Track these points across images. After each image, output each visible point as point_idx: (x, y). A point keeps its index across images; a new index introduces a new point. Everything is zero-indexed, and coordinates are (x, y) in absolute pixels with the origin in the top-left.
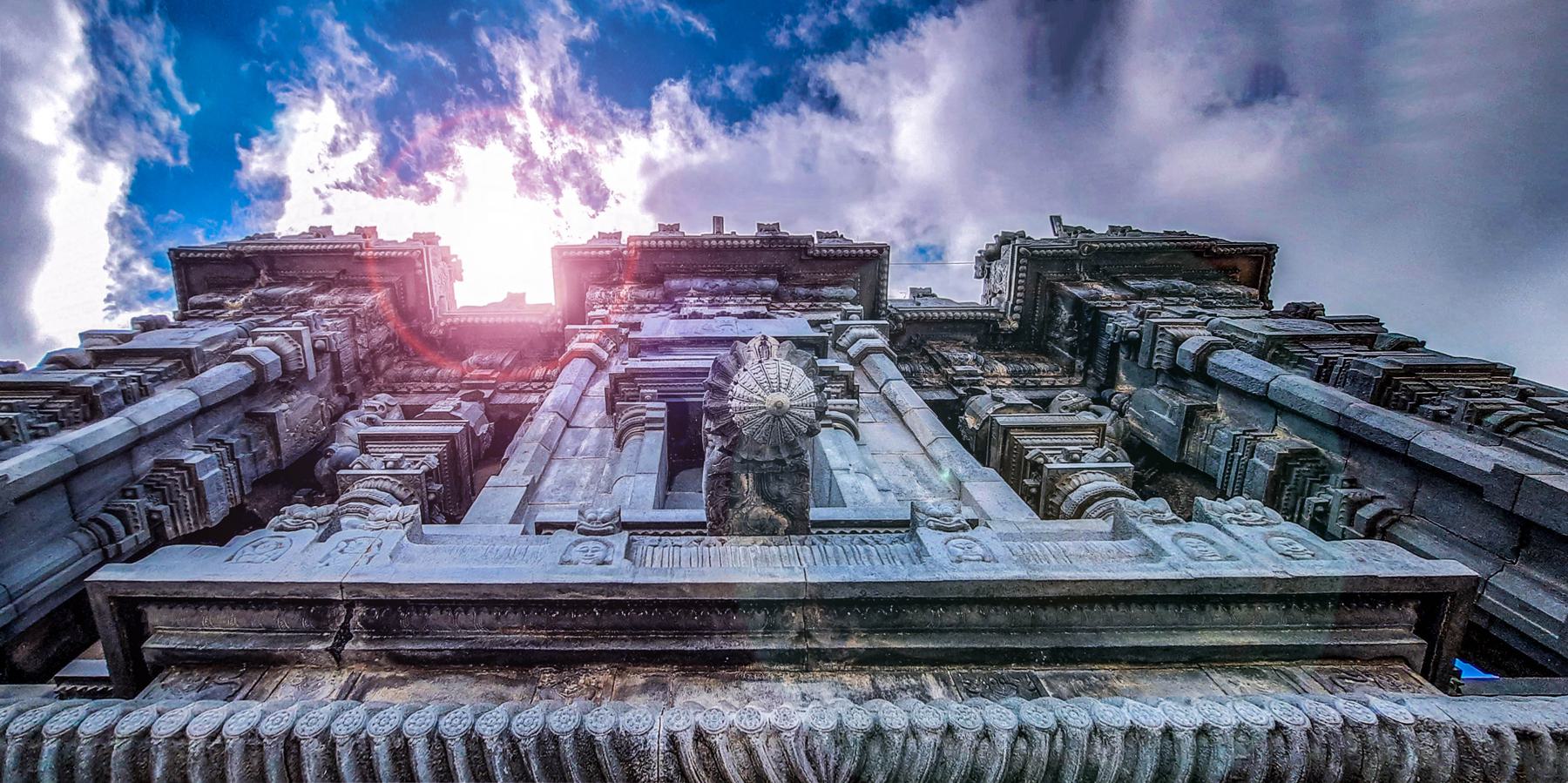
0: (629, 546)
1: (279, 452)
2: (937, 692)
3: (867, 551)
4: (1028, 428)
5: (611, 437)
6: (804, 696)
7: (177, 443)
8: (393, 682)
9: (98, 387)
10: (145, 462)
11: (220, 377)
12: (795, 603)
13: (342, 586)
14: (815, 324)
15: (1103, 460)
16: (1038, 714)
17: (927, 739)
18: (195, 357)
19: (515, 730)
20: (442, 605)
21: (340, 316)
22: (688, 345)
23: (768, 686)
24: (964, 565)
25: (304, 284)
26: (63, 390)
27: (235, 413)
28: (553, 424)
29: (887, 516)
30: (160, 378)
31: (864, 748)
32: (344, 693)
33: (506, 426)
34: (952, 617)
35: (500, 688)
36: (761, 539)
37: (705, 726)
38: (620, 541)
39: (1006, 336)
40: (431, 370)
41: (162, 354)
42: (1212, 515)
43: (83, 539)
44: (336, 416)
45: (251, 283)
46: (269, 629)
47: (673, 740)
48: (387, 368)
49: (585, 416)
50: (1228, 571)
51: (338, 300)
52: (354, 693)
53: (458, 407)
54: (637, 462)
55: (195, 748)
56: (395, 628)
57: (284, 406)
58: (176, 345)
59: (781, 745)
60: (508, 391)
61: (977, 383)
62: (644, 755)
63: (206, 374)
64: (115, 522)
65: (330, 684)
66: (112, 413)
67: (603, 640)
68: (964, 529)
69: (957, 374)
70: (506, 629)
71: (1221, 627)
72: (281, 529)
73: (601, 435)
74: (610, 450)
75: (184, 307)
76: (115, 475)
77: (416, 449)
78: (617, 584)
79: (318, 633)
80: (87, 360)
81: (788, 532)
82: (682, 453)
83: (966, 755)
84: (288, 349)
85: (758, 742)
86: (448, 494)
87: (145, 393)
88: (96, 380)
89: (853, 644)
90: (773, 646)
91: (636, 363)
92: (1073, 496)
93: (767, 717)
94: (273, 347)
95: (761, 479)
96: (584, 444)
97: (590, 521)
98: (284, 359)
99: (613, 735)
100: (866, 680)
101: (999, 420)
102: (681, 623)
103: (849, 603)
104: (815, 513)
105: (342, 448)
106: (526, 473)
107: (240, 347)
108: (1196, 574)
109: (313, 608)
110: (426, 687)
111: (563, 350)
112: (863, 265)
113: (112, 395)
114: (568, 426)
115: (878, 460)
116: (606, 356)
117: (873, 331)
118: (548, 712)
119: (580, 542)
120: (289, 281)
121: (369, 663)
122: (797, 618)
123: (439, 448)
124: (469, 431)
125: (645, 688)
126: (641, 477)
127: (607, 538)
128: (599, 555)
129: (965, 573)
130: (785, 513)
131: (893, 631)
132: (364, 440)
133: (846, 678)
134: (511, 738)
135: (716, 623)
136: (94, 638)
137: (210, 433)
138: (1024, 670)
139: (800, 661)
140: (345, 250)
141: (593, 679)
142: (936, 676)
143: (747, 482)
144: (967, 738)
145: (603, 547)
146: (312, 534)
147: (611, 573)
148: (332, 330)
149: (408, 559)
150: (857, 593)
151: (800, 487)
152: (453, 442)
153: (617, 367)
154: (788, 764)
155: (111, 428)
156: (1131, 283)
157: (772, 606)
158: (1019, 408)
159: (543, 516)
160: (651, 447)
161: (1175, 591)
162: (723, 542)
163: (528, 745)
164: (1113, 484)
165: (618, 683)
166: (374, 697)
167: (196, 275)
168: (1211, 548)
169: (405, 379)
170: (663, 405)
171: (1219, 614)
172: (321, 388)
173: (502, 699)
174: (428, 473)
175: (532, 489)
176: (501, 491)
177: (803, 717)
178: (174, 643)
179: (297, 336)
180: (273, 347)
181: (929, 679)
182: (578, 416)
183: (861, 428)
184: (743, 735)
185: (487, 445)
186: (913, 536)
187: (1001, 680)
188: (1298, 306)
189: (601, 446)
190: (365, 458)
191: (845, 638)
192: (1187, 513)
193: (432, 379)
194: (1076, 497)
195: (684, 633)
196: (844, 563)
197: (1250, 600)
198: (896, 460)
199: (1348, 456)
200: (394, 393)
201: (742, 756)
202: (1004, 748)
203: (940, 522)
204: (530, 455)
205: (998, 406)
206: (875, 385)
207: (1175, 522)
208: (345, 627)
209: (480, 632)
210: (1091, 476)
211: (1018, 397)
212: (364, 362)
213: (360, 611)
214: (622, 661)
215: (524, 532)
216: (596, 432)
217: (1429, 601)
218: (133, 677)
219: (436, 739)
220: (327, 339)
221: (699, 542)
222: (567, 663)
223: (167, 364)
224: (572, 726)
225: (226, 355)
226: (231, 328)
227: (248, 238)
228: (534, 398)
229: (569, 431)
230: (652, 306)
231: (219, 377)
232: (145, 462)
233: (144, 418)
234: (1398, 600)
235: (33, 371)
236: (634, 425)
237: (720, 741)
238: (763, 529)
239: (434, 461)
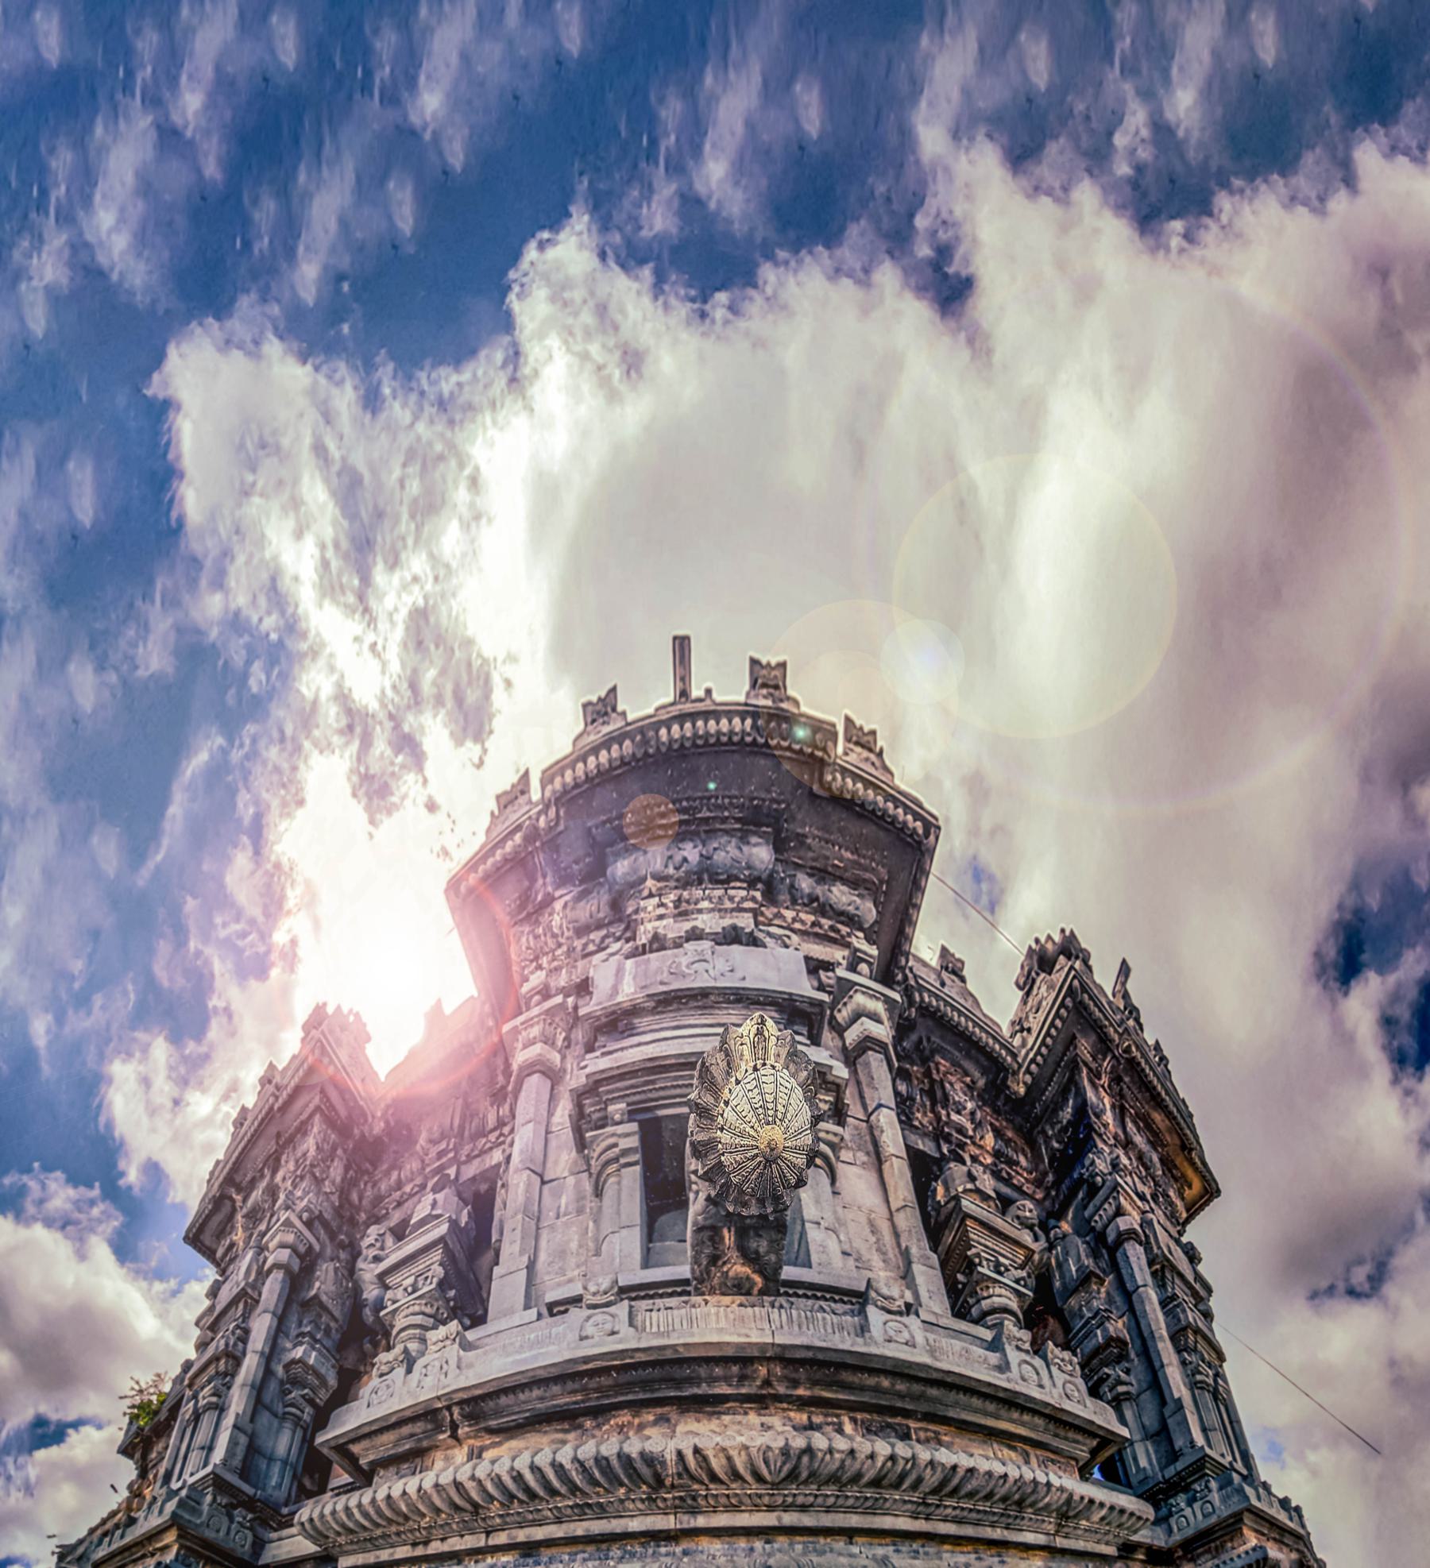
0: (630, 1313)
1: (336, 1320)
2: (848, 1428)
3: (824, 1319)
4: (982, 1224)
5: (588, 1187)
6: (762, 1425)
7: (284, 1350)
8: (494, 1445)
9: (227, 1345)
10: (280, 1370)
11: (271, 1290)
12: (763, 1359)
13: (438, 1398)
14: (815, 967)
15: (1017, 1281)
16: (902, 1450)
17: (837, 1456)
18: (249, 1291)
19: (580, 1457)
20: (506, 1391)
21: (302, 1178)
22: (653, 1011)
23: (739, 1418)
24: (892, 1345)
25: (262, 1176)
26: (216, 1359)
27: (295, 1307)
28: (529, 1185)
29: (844, 1284)
30: (246, 1317)
31: (799, 1458)
32: (470, 1458)
33: (482, 1202)
34: (871, 1381)
35: (560, 1436)
36: (739, 1299)
37: (700, 1445)
38: (622, 1309)
39: (1008, 1098)
40: (394, 1175)
41: (234, 1302)
42: (1050, 1355)
43: (288, 1425)
44: (351, 1270)
45: (234, 1211)
46: (412, 1435)
47: (680, 1454)
48: (361, 1199)
49: (556, 1162)
50: (1036, 1393)
51: (291, 1166)
52: (476, 1454)
53: (434, 1204)
54: (618, 1213)
55: (414, 1496)
56: (482, 1411)
57: (317, 1284)
58: (235, 1291)
59: (749, 1455)
60: (470, 1158)
61: (962, 1146)
62: (663, 1463)
63: (263, 1297)
64: (293, 1410)
65: (460, 1455)
66: (244, 1354)
67: (622, 1394)
68: (900, 1313)
69: (949, 1123)
70: (553, 1397)
71: (1013, 1421)
72: (381, 1375)
73: (577, 1184)
74: (590, 1203)
75: (217, 1264)
76: (273, 1386)
77: (419, 1266)
78: (627, 1350)
79: (439, 1429)
80: (210, 1334)
81: (763, 1292)
82: (663, 1196)
83: (857, 1465)
84: (290, 1238)
85: (734, 1453)
86: (465, 1299)
87: (247, 1332)
88: (222, 1342)
89: (801, 1392)
90: (744, 1391)
91: (598, 1063)
92: (983, 1303)
93: (740, 1439)
94: (282, 1246)
95: (742, 1233)
96: (563, 1201)
97: (594, 1294)
98: (294, 1250)
99: (642, 1454)
100: (805, 1417)
101: (964, 1202)
102: (677, 1376)
103: (802, 1362)
104: (789, 1272)
105: (371, 1293)
106: (521, 1253)
107: (265, 1262)
108: (1018, 1388)
109: (429, 1415)
110: (515, 1444)
111: (507, 1072)
112: (893, 845)
113: (235, 1344)
114: (543, 1183)
115: (849, 1215)
116: (556, 1058)
117: (879, 1007)
118: (598, 1445)
119: (589, 1317)
120: (253, 1183)
121: (475, 1437)
122: (763, 1371)
123: (437, 1255)
124: (454, 1223)
125: (655, 1423)
126: (624, 1232)
127: (612, 1309)
128: (608, 1327)
129: (890, 1351)
130: (761, 1272)
131: (828, 1385)
132: (382, 1277)
133: (792, 1414)
134: (579, 1461)
136: (330, 1463)
137: (293, 1332)
138: (904, 1422)
139: (761, 1401)
140: (267, 1114)
141: (619, 1421)
142: (851, 1418)
143: (728, 1237)
144: (861, 1456)
145: (609, 1318)
146: (400, 1371)
147: (620, 1341)
148: (306, 1198)
149: (470, 1366)
150: (810, 1354)
151: (776, 1246)
152: (446, 1244)
153: (576, 1079)
154: (752, 1465)
155: (250, 1364)
157: (742, 1360)
158: (985, 1197)
159: (550, 1297)
160: (628, 1185)
161: (1001, 1395)
162: (706, 1302)
163: (590, 1463)
164: (1014, 1305)
165: (637, 1421)
166: (488, 1455)
167: (207, 1238)
168: (1035, 1377)
169: (378, 1199)
170: (634, 1127)
171: (1016, 1415)
172: (329, 1251)
173: (564, 1442)
174: (441, 1284)
175: (531, 1267)
176: (506, 1286)
177: (759, 1440)
178: (372, 1458)
179: (288, 1223)
180: (282, 1246)
181: (846, 1419)
182: (549, 1165)
183: (841, 1168)
184: (724, 1450)
185: (473, 1233)
186: (862, 1312)
187: (889, 1425)
188: (1193, 1248)
189: (580, 1198)
190: (389, 1294)
191: (795, 1387)
192: (1037, 1349)
193: (399, 1185)
194: (985, 1304)
195: (678, 1383)
196: (804, 1328)
197: (1035, 1412)
198: (863, 1220)
200: (377, 1220)
201: (724, 1461)
202: (879, 1464)
203: (886, 1304)
204: (518, 1232)
205: (969, 1186)
206: (864, 1106)
207: (1027, 1352)
208: (452, 1421)
209: (534, 1401)
210: (1003, 1292)
211: (987, 1183)
212: (341, 1206)
213: (456, 1411)
214: (637, 1406)
215: (540, 1316)
216: (571, 1180)
217: (1105, 1439)
218: (365, 1477)
219: (534, 1468)
220: (307, 1209)
221: (686, 1302)
222: (599, 1413)
223: (241, 1306)
224: (615, 1451)
225: (263, 1275)
226: (250, 1255)
227: (209, 1181)
228: (497, 1156)
229: (546, 1187)
230: (596, 936)
231: (271, 1291)
232: (280, 1370)
233: (259, 1346)
234: (1092, 1435)
235: (198, 1359)
236: (608, 1163)
237: (710, 1453)
238: (740, 1288)
239: (439, 1271)
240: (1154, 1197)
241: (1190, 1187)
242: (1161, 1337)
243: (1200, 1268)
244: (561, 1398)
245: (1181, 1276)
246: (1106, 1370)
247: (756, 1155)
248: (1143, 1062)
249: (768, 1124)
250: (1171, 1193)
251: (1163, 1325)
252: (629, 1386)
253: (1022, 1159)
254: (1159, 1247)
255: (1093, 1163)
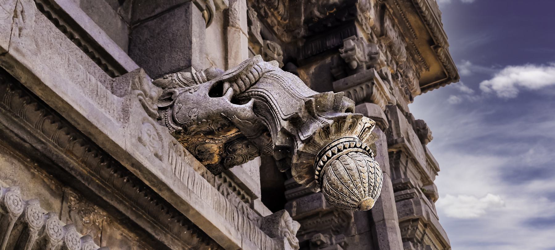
70: (69, 152)
81: (209, 167)
135: (176, 230)
156: (388, 23)
188: (425, 128)
195: (156, 222)
199: (360, 234)
240: (395, 77)
241: (428, 69)
242: (393, 228)
243: (428, 146)
244: (74, 160)
245: (416, 163)
246: (322, 237)
247: (356, 202)
248: (433, 25)
249: (372, 196)
250: (410, 75)
251: (396, 215)
252: (124, 197)
253: (281, 9)
254: (399, 134)
255: (353, 49)
